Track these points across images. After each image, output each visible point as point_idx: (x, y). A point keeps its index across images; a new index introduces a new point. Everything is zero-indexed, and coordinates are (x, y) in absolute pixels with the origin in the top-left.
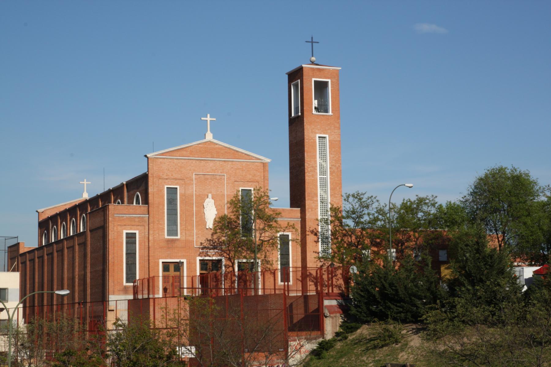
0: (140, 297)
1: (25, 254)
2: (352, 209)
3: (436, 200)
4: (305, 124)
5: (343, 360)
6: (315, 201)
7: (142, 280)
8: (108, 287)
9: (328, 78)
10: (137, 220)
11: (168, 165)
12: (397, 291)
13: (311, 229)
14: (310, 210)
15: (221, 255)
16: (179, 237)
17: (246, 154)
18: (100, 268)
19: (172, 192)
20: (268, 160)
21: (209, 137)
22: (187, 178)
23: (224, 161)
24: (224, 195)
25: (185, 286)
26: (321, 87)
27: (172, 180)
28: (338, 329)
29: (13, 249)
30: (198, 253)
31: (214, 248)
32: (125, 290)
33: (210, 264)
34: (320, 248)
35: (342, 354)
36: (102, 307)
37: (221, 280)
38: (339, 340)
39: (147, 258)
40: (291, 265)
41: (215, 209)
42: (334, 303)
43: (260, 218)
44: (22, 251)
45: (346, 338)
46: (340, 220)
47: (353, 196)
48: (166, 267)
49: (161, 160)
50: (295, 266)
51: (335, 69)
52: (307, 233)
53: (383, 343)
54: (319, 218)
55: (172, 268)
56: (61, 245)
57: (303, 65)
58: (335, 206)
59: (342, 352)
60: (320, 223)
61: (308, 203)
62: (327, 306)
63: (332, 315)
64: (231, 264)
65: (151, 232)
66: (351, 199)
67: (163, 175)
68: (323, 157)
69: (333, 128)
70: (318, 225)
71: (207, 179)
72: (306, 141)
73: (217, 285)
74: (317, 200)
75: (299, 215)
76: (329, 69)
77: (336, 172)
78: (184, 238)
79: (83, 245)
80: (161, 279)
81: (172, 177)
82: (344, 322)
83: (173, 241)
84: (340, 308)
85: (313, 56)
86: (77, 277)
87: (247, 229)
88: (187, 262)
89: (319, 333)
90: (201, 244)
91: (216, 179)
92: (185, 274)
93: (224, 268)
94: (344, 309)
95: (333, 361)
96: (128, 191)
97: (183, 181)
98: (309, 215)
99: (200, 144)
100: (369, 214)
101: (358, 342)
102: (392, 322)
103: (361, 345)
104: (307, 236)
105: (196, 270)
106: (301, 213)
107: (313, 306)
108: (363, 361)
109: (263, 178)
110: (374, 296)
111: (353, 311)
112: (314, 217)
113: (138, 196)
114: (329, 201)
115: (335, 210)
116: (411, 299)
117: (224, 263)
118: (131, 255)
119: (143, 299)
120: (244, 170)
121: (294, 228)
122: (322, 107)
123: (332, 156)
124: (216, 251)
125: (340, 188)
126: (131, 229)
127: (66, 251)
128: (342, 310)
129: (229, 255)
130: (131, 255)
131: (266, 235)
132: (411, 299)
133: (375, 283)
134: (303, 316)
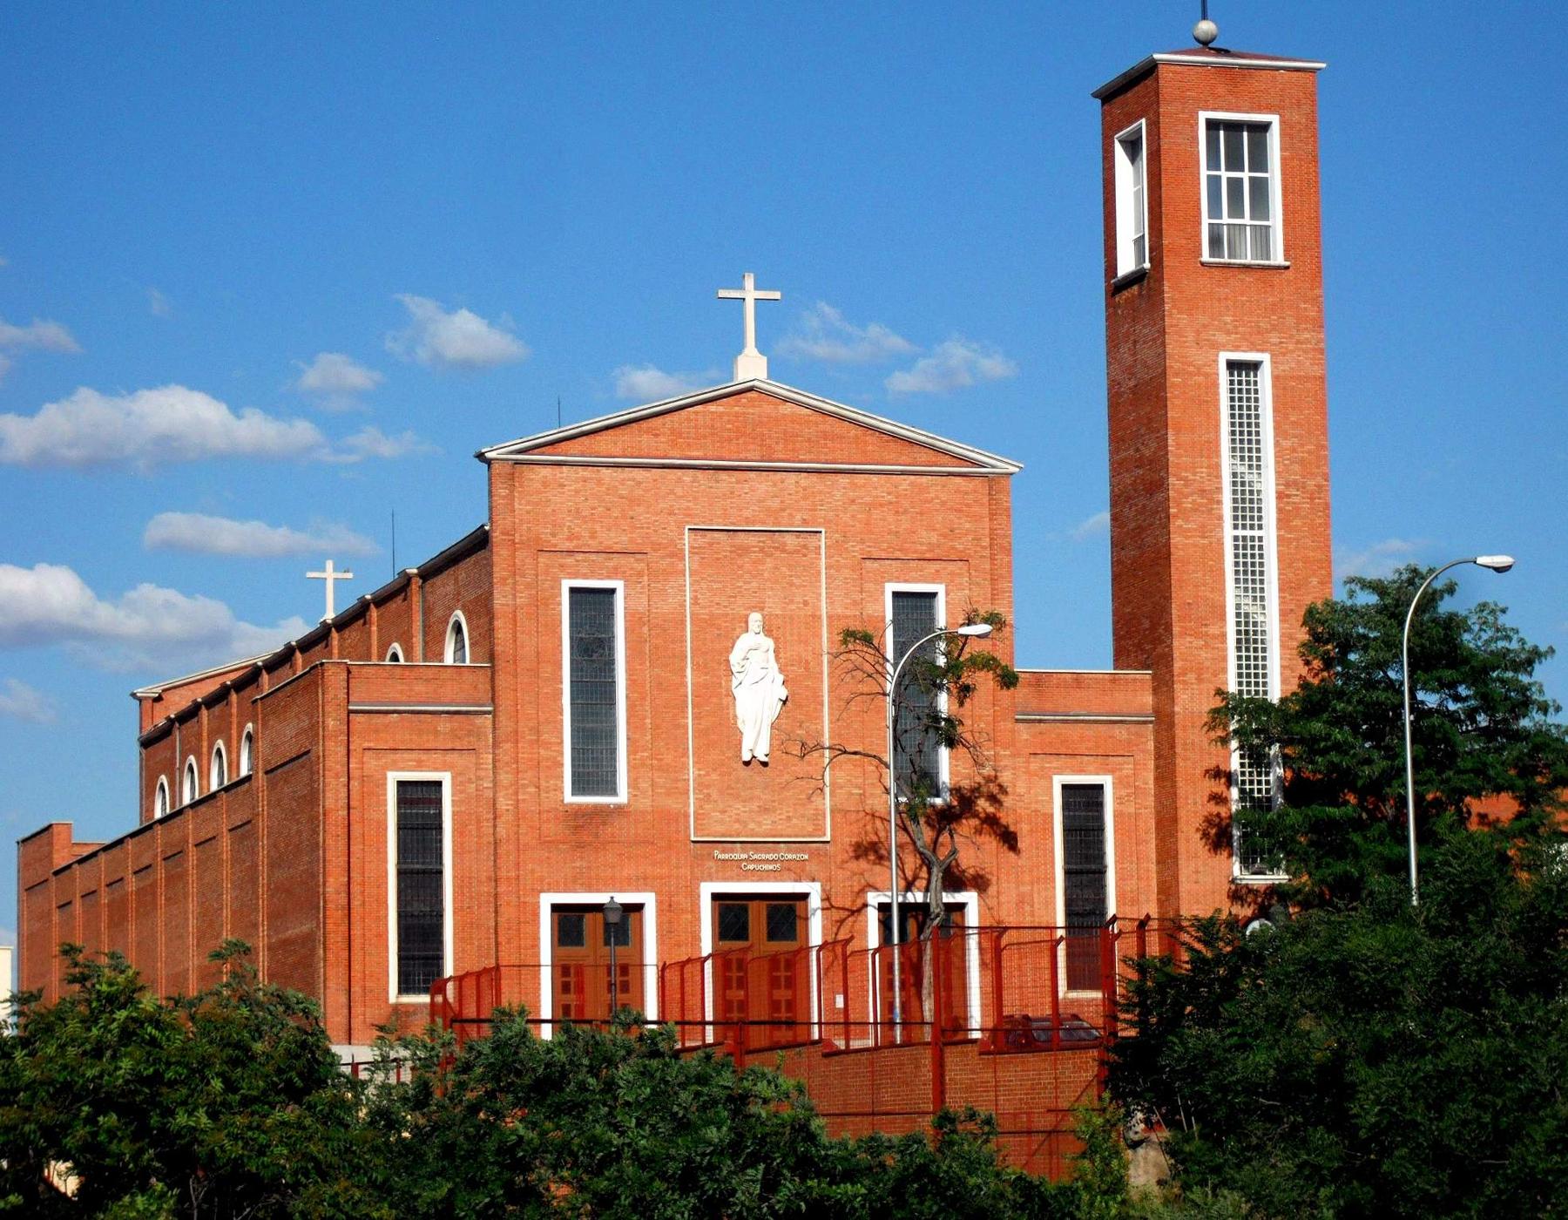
6: (1214, 637)
9: (1269, 109)
11: (577, 492)
14: (1191, 677)
16: (622, 797)
22: (657, 547)
27: (593, 557)
67: (554, 535)
69: (1290, 321)
81: (594, 545)
97: (642, 560)
109: (986, 542)
120: (906, 512)
126: (419, 766)
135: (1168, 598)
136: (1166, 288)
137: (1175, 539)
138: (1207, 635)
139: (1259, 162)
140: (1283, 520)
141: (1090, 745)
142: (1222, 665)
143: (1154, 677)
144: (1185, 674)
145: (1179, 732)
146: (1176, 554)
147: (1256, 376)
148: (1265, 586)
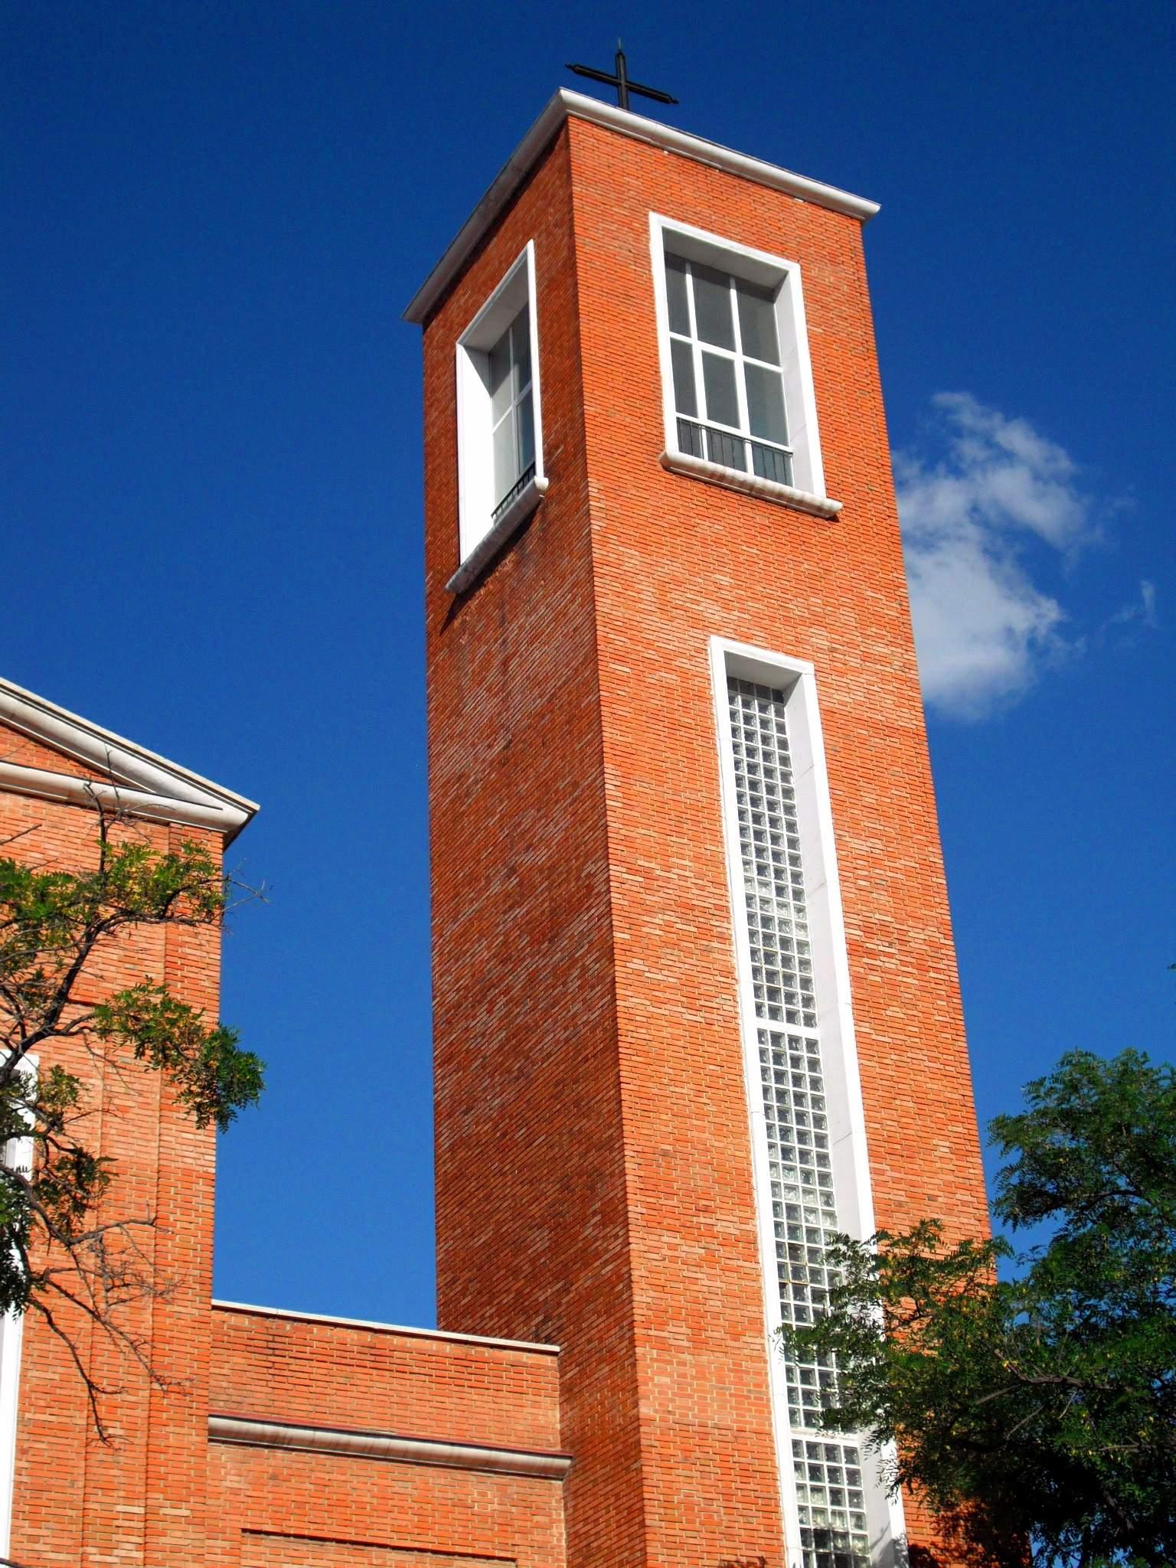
4: (596, 526)
8: (161, 759)
14: (677, 1333)
55: (822, 1452)
123: (859, 845)
135: (613, 1144)
136: (593, 491)
137: (629, 1000)
138: (710, 1232)
139: (761, 342)
140: (865, 1005)
141: (409, 1520)
142: (750, 1311)
143: (565, 1361)
144: (662, 1325)
145: (653, 1473)
146: (629, 1034)
147: (780, 713)
148: (830, 1150)
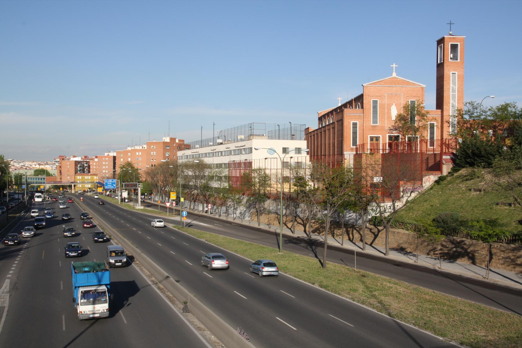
0: (359, 153)
1: (311, 132)
2: (468, 110)
3: (516, 104)
5: (450, 186)
7: (359, 145)
10: (358, 116)
12: (480, 151)
13: (446, 120)
15: (399, 133)
16: (378, 124)
17: (413, 83)
18: (341, 139)
19: (375, 102)
20: (425, 86)
21: (394, 75)
23: (402, 87)
24: (401, 104)
25: (381, 148)
26: (454, 48)
28: (450, 170)
29: (307, 130)
30: (388, 132)
31: (396, 130)
32: (352, 150)
33: (393, 138)
34: (451, 129)
35: (450, 183)
36: (341, 157)
37: (399, 146)
38: (450, 176)
39: (362, 135)
40: (435, 138)
41: (397, 111)
42: (448, 157)
43: (419, 115)
44: (310, 131)
45: (453, 175)
46: (462, 116)
47: (469, 103)
48: (372, 139)
49: (370, 87)
50: (437, 139)
51: (462, 37)
52: (444, 122)
53: (471, 178)
54: (451, 114)
55: (374, 139)
56: (325, 128)
57: (445, 36)
58: (459, 108)
59: (450, 182)
60: (451, 117)
61: (445, 107)
62: (444, 159)
63: (447, 163)
64: (404, 138)
65: (364, 122)
66: (468, 105)
68: (454, 84)
70: (450, 118)
71: (393, 96)
72: (445, 75)
73: (397, 148)
74: (450, 106)
75: (440, 113)
76: (459, 38)
77: (461, 92)
78: (380, 125)
79: (334, 128)
80: (369, 145)
82: (454, 167)
83: (375, 126)
84: (451, 160)
85: (450, 31)
86: (331, 143)
87: (412, 120)
88: (382, 136)
89: (440, 172)
90: (389, 128)
91: (397, 96)
92: (381, 142)
93: (400, 140)
94: (453, 160)
95: (445, 186)
96: (355, 103)
98: (445, 113)
99: (389, 79)
100: (477, 112)
101: (459, 177)
102: (477, 167)
103: (460, 179)
104: (444, 124)
105: (386, 140)
106: (441, 112)
107: (438, 159)
108: (460, 186)
110: (469, 154)
111: (458, 161)
112: (448, 114)
113: (359, 105)
114: (456, 106)
115: (459, 110)
116: (487, 155)
117: (400, 137)
118: (355, 133)
119: (360, 154)
121: (436, 120)
122: (455, 58)
124: (396, 131)
125: (463, 99)
126: (355, 121)
127: (327, 131)
128: (452, 161)
129: (403, 133)
130: (355, 133)
131: (421, 124)
132: (487, 155)
133: (469, 147)
134: (433, 163)
